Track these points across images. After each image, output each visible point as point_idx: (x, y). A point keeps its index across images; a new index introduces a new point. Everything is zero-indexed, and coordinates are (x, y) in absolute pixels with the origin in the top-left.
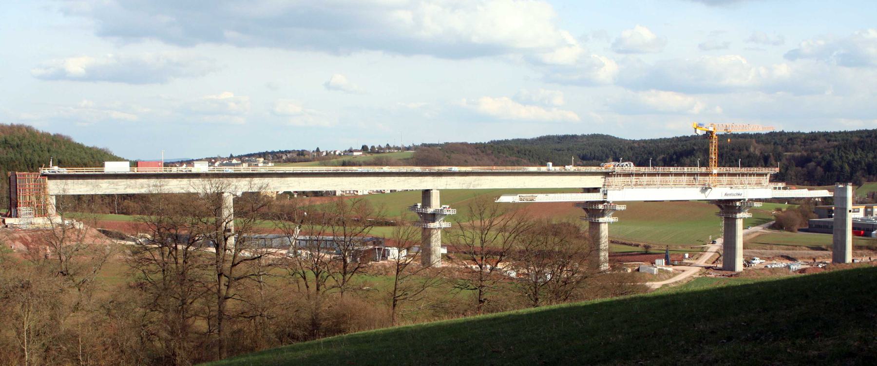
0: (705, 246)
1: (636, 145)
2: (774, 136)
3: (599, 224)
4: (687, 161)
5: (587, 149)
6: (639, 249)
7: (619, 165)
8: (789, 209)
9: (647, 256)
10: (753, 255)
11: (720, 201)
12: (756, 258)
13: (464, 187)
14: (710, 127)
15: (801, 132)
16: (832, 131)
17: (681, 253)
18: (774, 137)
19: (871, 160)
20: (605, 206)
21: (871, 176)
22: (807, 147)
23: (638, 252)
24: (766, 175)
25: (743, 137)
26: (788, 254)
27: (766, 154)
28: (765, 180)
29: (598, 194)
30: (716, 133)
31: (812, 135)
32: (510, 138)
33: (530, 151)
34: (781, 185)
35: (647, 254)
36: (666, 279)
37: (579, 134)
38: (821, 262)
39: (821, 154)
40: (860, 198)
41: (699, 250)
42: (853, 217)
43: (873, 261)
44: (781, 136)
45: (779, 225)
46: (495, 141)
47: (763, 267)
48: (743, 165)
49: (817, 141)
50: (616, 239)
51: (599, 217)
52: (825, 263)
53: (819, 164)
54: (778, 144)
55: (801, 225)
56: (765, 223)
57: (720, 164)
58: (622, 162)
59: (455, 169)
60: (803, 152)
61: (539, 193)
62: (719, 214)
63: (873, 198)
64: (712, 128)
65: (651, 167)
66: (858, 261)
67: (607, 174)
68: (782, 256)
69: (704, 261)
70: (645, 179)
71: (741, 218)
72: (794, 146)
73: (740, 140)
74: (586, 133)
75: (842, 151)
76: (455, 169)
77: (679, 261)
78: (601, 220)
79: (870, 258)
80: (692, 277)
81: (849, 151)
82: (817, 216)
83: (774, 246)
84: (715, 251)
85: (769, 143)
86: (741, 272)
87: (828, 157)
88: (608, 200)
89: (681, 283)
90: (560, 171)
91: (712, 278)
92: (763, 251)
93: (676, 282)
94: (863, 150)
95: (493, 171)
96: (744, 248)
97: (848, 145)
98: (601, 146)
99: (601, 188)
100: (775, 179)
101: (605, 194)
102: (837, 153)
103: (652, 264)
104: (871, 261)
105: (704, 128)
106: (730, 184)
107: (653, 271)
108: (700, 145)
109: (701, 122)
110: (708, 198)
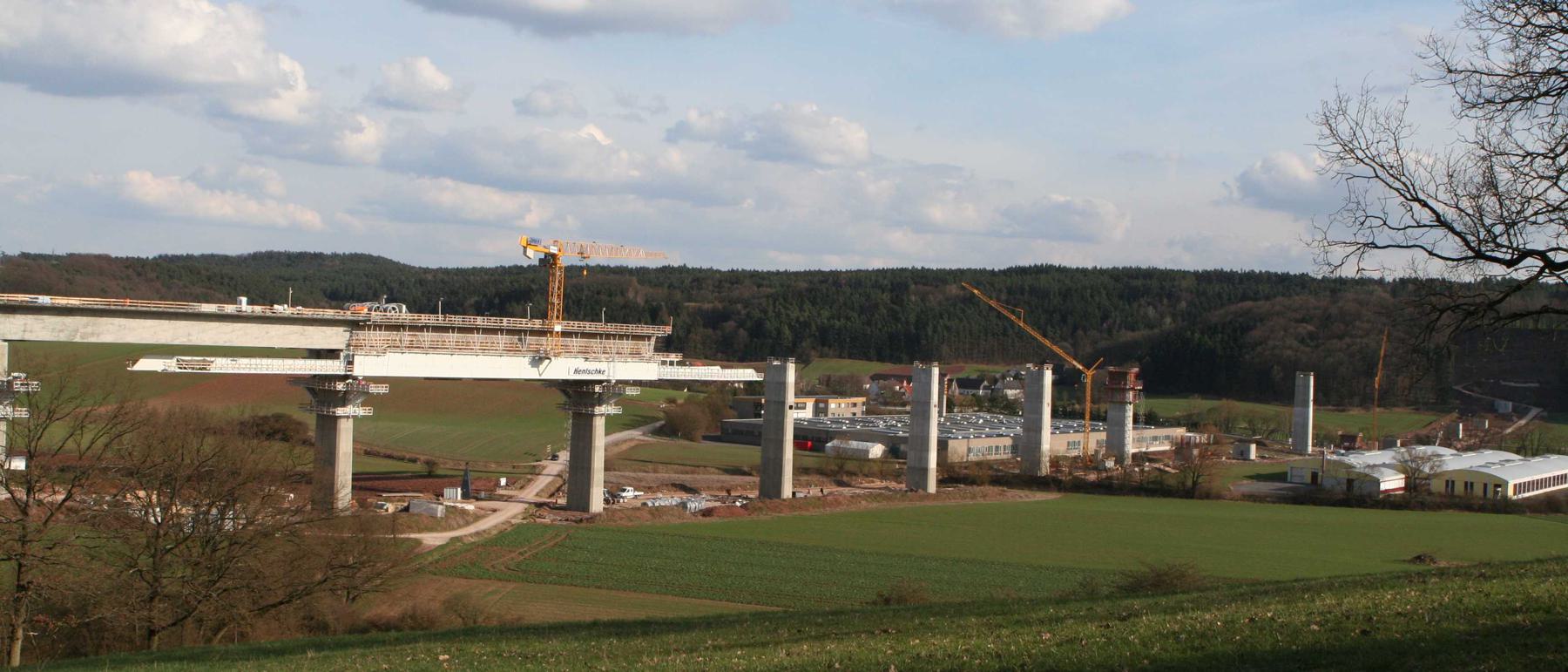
0: (539, 463)
1: (430, 277)
2: (670, 273)
3: (336, 419)
4: (518, 308)
5: (341, 280)
6: (418, 467)
7: (378, 307)
8: (689, 400)
9: (431, 480)
10: (623, 481)
11: (566, 383)
12: (628, 488)
13: (63, 337)
14: (552, 247)
15: (715, 268)
16: (765, 270)
17: (493, 476)
18: (669, 275)
19: (826, 321)
20: (348, 384)
21: (826, 349)
22: (724, 294)
23: (412, 472)
24: (649, 338)
25: (617, 273)
26: (683, 481)
27: (655, 304)
28: (647, 347)
29: (336, 362)
30: (563, 262)
31: (732, 274)
32: (197, 252)
33: (232, 278)
34: (674, 357)
35: (431, 479)
36: (460, 527)
37: (327, 251)
38: (740, 497)
39: (745, 307)
40: (808, 385)
41: (526, 471)
42: (795, 416)
43: (827, 495)
44: (681, 273)
45: (671, 428)
46: (166, 256)
47: (639, 505)
48: (610, 320)
49: (739, 286)
50: (376, 448)
51: (335, 407)
52: (746, 498)
53: (741, 325)
54: (675, 288)
55: (707, 429)
56: (648, 424)
57: (569, 313)
58: (386, 303)
59: (45, 300)
60: (716, 303)
61: (220, 356)
62: (563, 407)
63: (827, 385)
64: (556, 248)
65: (440, 315)
66: (802, 495)
67: (354, 325)
68: (674, 485)
69: (534, 493)
70: (428, 337)
71: (602, 415)
72: (702, 292)
73: (612, 276)
74: (340, 251)
75: (780, 304)
76: (45, 300)
77: (488, 491)
78: (340, 411)
79: (822, 491)
80: (510, 522)
81: (791, 304)
82: (736, 413)
83: (661, 467)
84: (555, 473)
85: (661, 285)
86: (600, 514)
87: (757, 314)
88: (355, 373)
89: (486, 536)
90: (263, 314)
91: (545, 526)
92: (641, 475)
93: (477, 533)
94: (814, 304)
95: (125, 308)
96: (606, 469)
97: (790, 295)
98: (367, 276)
99: (342, 350)
100: (665, 346)
101: (350, 363)
102: (771, 307)
103: (438, 496)
104: (824, 496)
105: (540, 248)
106: (585, 353)
107: (437, 510)
108: (542, 282)
109: (535, 237)
110: (542, 377)
